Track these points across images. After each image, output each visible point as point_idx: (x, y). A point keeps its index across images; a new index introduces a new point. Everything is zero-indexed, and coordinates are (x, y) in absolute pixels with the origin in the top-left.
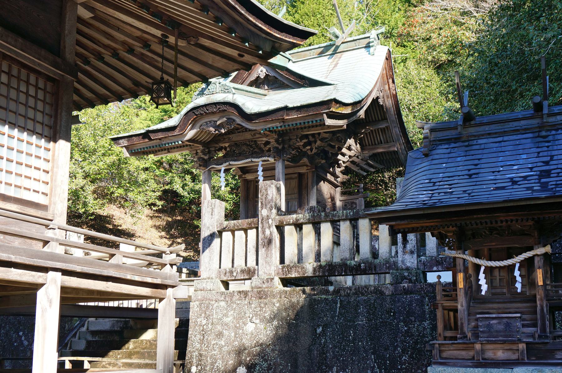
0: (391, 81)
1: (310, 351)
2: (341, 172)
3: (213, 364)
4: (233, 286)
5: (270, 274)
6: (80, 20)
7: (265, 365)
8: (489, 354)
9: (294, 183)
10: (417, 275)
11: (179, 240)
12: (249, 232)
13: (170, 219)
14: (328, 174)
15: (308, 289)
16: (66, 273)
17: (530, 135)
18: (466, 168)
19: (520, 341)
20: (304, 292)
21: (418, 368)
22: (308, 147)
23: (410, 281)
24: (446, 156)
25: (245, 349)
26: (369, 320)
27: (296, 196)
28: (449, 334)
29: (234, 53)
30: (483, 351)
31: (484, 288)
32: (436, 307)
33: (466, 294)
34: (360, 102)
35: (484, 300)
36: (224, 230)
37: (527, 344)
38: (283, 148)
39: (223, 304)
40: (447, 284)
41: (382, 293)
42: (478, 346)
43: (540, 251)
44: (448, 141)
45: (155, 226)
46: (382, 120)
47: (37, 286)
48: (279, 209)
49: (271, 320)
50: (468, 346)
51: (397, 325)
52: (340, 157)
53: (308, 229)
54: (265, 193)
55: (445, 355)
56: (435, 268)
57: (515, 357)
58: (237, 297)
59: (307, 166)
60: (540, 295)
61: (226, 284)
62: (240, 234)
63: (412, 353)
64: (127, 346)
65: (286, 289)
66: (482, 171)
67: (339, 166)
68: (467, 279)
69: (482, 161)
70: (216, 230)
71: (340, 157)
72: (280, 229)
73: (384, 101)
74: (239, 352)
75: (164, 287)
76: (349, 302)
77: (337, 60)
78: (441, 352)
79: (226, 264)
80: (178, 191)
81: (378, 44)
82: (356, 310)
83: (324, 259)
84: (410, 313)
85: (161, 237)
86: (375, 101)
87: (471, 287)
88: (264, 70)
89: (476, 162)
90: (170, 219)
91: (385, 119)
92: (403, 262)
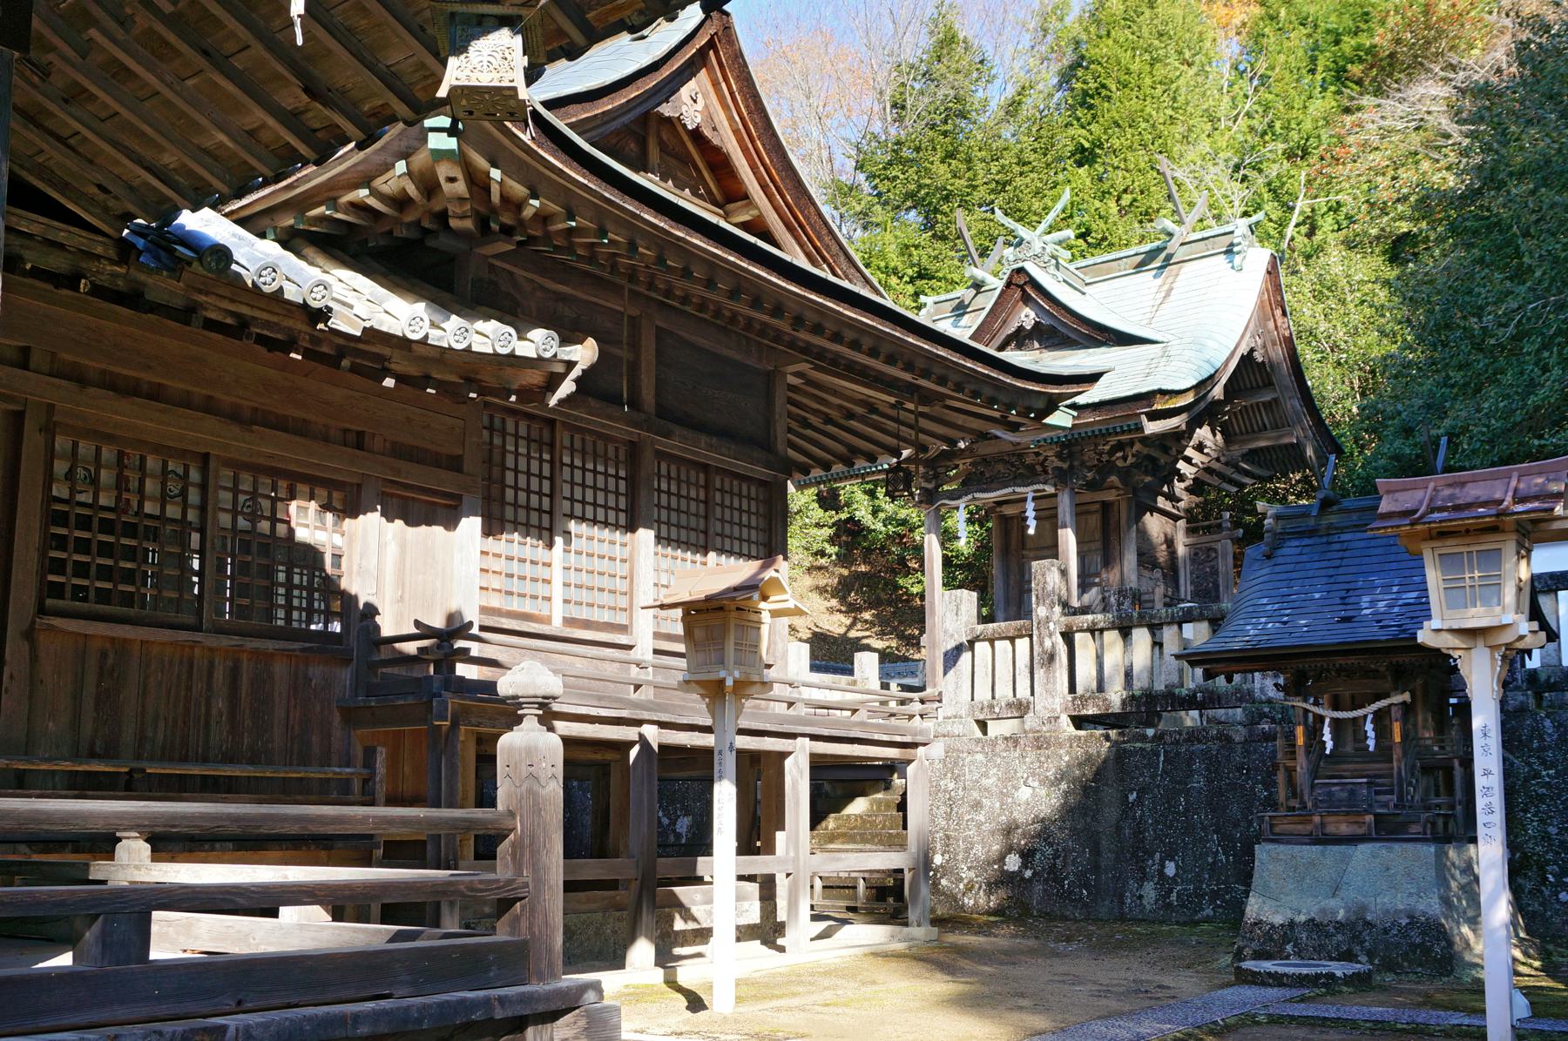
0: (1278, 312)
1: (1119, 829)
3: (967, 850)
4: (994, 729)
5: (1053, 710)
6: (792, 388)
7: (1050, 851)
8: (1331, 829)
9: (1094, 521)
11: (867, 615)
12: (1018, 641)
13: (845, 572)
15: (1113, 733)
16: (814, 737)
20: (1107, 738)
22: (1120, 454)
23: (1273, 721)
25: (1017, 827)
26: (1210, 781)
27: (1099, 545)
30: (1323, 825)
31: (1329, 745)
34: (1211, 377)
36: (977, 639)
38: (1071, 467)
39: (980, 757)
41: (1229, 739)
42: (1317, 819)
43: (1397, 699)
44: (1300, 534)
45: (817, 587)
46: (1265, 386)
47: (783, 755)
48: (1065, 605)
49: (1056, 782)
50: (1305, 818)
51: (1252, 789)
52: (1181, 465)
53: (1112, 636)
55: (1277, 830)
57: (1361, 831)
58: (1001, 746)
61: (983, 725)
62: (1003, 646)
64: (824, 824)
65: (1082, 733)
70: (964, 640)
71: (1181, 465)
72: (1068, 637)
74: (1008, 831)
75: (914, 745)
76: (1178, 754)
77: (1170, 280)
79: (983, 694)
80: (864, 521)
81: (1251, 245)
82: (1189, 765)
83: (1139, 684)
85: (831, 610)
86: (1247, 359)
88: (1032, 315)
90: (845, 572)
91: (1269, 384)
92: (1262, 690)
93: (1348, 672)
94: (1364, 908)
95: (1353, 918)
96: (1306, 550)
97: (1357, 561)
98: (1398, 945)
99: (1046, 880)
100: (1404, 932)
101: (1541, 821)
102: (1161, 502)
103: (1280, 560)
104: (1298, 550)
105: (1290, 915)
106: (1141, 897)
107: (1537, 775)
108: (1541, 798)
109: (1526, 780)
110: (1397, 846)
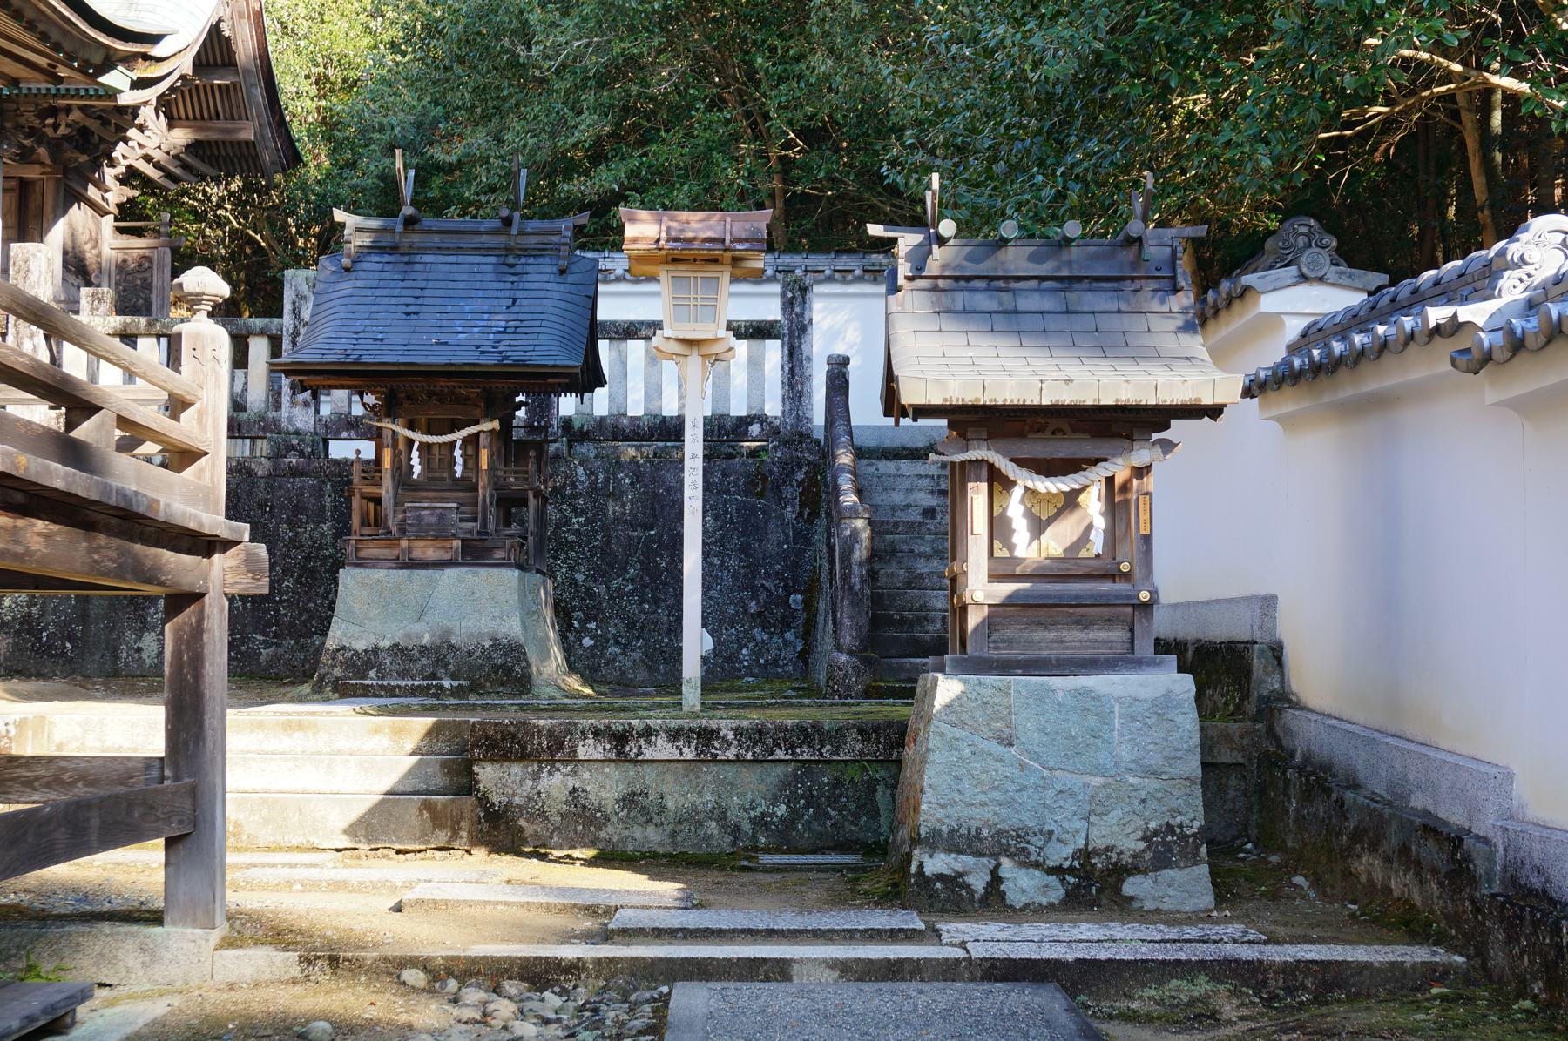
2: (117, 178)
8: (417, 554)
10: (314, 444)
14: (90, 186)
17: (493, 259)
18: (403, 300)
19: (454, 536)
21: (310, 600)
22: (50, 121)
23: (302, 454)
24: (377, 275)
28: (367, 531)
29: (43, 62)
31: (417, 470)
32: (351, 493)
33: (393, 477)
35: (414, 487)
37: (463, 540)
40: (368, 462)
41: (251, 473)
46: (224, 65)
51: (277, 527)
54: (24, 268)
55: (362, 554)
56: (344, 435)
57: (447, 556)
59: (42, 164)
60: (483, 481)
63: (300, 576)
66: (424, 309)
67: (112, 165)
68: (396, 456)
69: (426, 293)
73: (233, 28)
78: (357, 550)
84: (298, 509)
87: (400, 468)
89: (418, 292)
92: (289, 419)
93: (440, 397)
94: (449, 632)
95: (438, 642)
96: (388, 267)
97: (442, 284)
98: (481, 667)
99: (18, 632)
100: (486, 654)
101: (570, 567)
102: (93, 192)
103: (362, 275)
104: (379, 267)
105: (373, 640)
106: (139, 650)
107: (568, 522)
108: (571, 545)
109: (558, 527)
110: (483, 571)
